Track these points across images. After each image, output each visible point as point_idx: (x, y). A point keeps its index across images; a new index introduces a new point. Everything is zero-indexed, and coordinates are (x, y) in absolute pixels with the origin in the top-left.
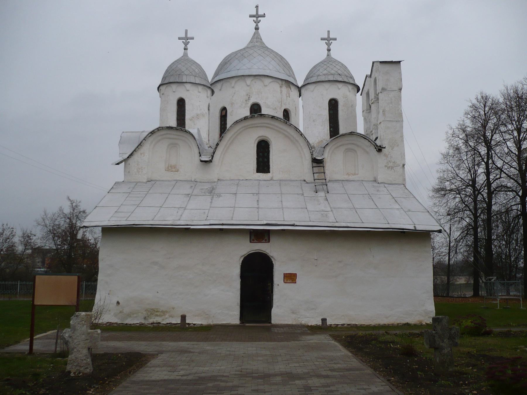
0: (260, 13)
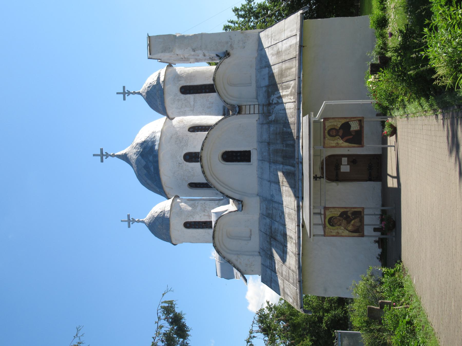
0: (99, 153)
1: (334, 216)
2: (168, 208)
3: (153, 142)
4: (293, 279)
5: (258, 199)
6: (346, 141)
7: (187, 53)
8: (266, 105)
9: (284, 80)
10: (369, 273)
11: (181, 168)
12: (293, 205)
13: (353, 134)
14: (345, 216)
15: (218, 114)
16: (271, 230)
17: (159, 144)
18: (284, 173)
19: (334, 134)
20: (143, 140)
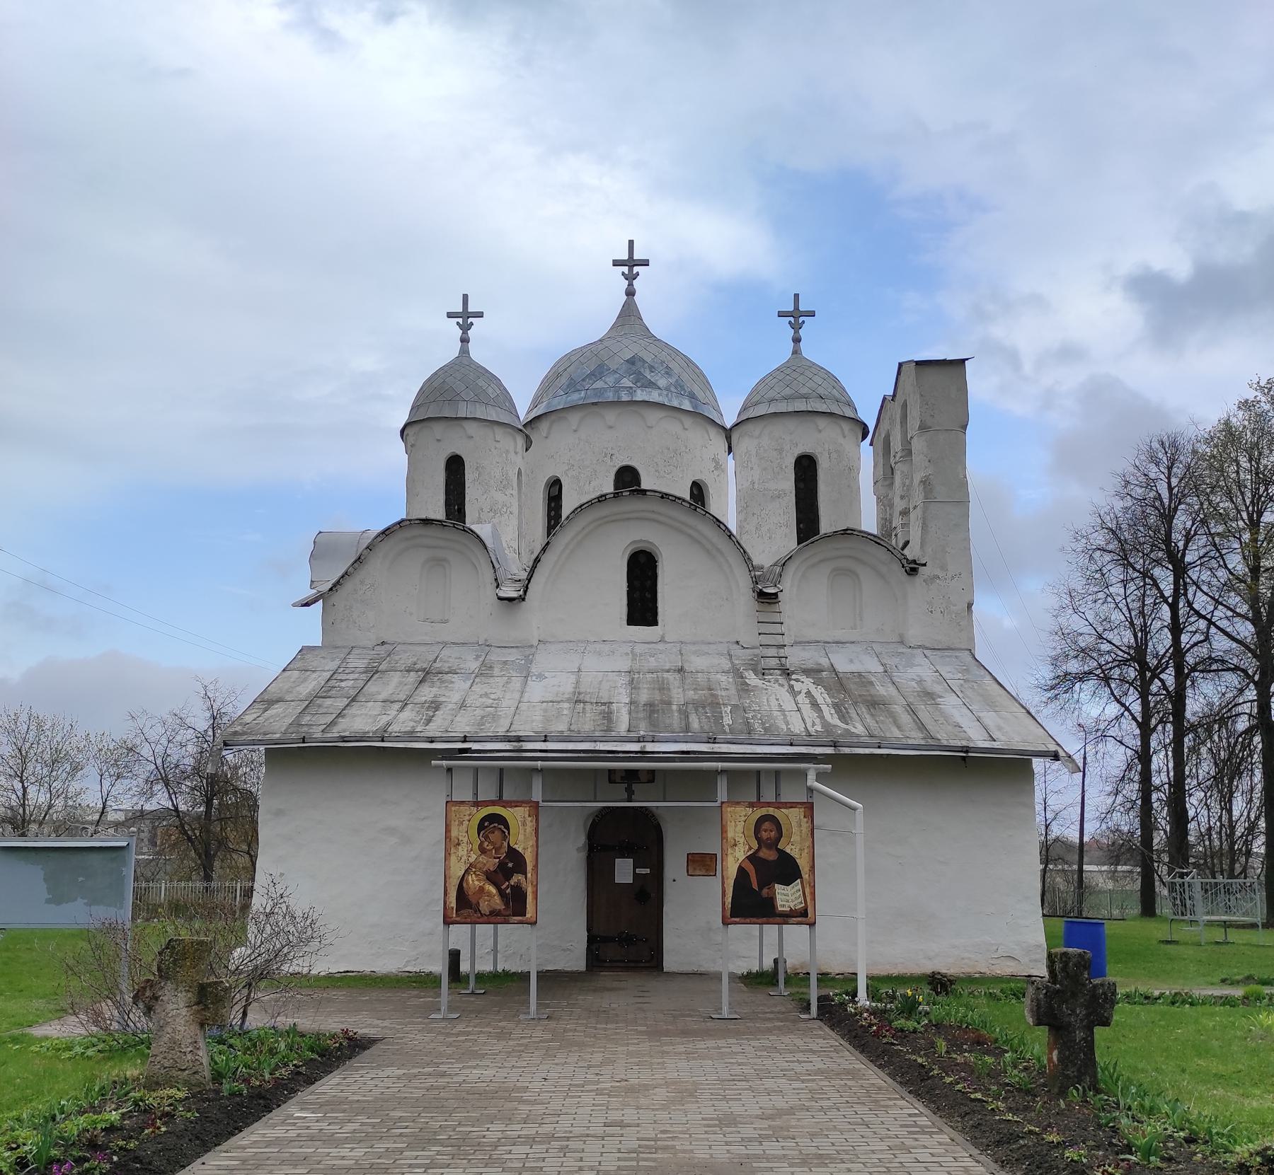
1: (509, 833)
4: (312, 725)
6: (741, 870)
11: (600, 460)
12: (522, 728)
13: (765, 892)
14: (510, 865)
16: (447, 673)
19: (764, 835)
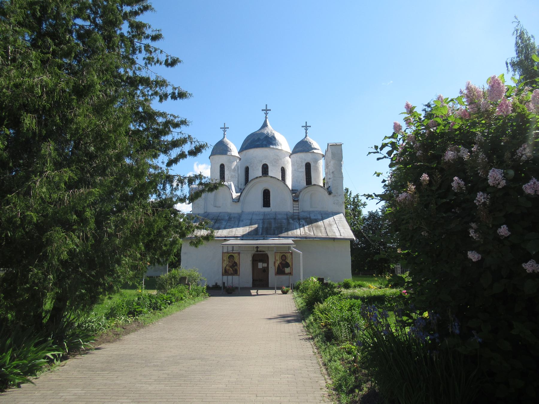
0: (268, 108)
2: (233, 154)
3: (275, 144)
5: (240, 211)
6: (279, 266)
7: (331, 167)
8: (298, 217)
9: (314, 228)
10: (203, 278)
15: (292, 186)
17: (274, 148)
18: (257, 228)
20: (276, 138)
